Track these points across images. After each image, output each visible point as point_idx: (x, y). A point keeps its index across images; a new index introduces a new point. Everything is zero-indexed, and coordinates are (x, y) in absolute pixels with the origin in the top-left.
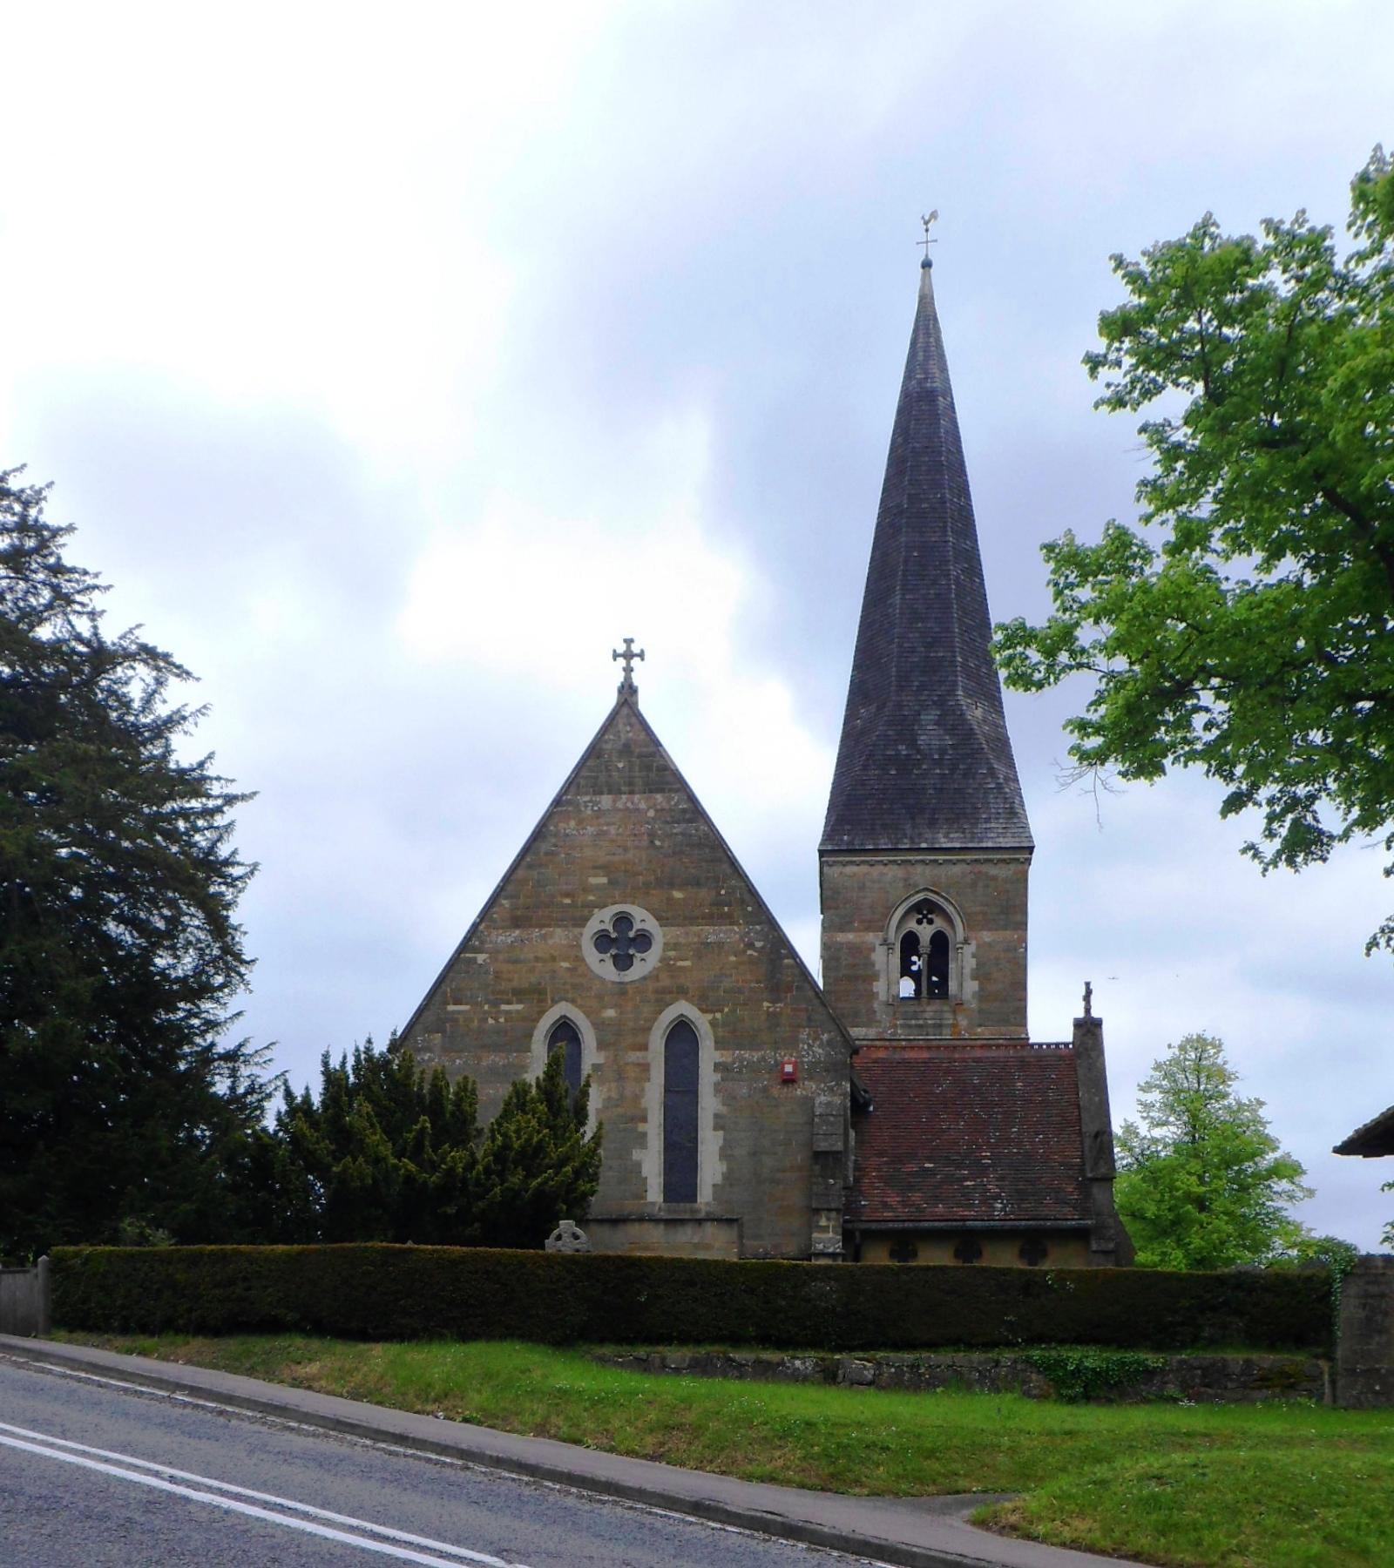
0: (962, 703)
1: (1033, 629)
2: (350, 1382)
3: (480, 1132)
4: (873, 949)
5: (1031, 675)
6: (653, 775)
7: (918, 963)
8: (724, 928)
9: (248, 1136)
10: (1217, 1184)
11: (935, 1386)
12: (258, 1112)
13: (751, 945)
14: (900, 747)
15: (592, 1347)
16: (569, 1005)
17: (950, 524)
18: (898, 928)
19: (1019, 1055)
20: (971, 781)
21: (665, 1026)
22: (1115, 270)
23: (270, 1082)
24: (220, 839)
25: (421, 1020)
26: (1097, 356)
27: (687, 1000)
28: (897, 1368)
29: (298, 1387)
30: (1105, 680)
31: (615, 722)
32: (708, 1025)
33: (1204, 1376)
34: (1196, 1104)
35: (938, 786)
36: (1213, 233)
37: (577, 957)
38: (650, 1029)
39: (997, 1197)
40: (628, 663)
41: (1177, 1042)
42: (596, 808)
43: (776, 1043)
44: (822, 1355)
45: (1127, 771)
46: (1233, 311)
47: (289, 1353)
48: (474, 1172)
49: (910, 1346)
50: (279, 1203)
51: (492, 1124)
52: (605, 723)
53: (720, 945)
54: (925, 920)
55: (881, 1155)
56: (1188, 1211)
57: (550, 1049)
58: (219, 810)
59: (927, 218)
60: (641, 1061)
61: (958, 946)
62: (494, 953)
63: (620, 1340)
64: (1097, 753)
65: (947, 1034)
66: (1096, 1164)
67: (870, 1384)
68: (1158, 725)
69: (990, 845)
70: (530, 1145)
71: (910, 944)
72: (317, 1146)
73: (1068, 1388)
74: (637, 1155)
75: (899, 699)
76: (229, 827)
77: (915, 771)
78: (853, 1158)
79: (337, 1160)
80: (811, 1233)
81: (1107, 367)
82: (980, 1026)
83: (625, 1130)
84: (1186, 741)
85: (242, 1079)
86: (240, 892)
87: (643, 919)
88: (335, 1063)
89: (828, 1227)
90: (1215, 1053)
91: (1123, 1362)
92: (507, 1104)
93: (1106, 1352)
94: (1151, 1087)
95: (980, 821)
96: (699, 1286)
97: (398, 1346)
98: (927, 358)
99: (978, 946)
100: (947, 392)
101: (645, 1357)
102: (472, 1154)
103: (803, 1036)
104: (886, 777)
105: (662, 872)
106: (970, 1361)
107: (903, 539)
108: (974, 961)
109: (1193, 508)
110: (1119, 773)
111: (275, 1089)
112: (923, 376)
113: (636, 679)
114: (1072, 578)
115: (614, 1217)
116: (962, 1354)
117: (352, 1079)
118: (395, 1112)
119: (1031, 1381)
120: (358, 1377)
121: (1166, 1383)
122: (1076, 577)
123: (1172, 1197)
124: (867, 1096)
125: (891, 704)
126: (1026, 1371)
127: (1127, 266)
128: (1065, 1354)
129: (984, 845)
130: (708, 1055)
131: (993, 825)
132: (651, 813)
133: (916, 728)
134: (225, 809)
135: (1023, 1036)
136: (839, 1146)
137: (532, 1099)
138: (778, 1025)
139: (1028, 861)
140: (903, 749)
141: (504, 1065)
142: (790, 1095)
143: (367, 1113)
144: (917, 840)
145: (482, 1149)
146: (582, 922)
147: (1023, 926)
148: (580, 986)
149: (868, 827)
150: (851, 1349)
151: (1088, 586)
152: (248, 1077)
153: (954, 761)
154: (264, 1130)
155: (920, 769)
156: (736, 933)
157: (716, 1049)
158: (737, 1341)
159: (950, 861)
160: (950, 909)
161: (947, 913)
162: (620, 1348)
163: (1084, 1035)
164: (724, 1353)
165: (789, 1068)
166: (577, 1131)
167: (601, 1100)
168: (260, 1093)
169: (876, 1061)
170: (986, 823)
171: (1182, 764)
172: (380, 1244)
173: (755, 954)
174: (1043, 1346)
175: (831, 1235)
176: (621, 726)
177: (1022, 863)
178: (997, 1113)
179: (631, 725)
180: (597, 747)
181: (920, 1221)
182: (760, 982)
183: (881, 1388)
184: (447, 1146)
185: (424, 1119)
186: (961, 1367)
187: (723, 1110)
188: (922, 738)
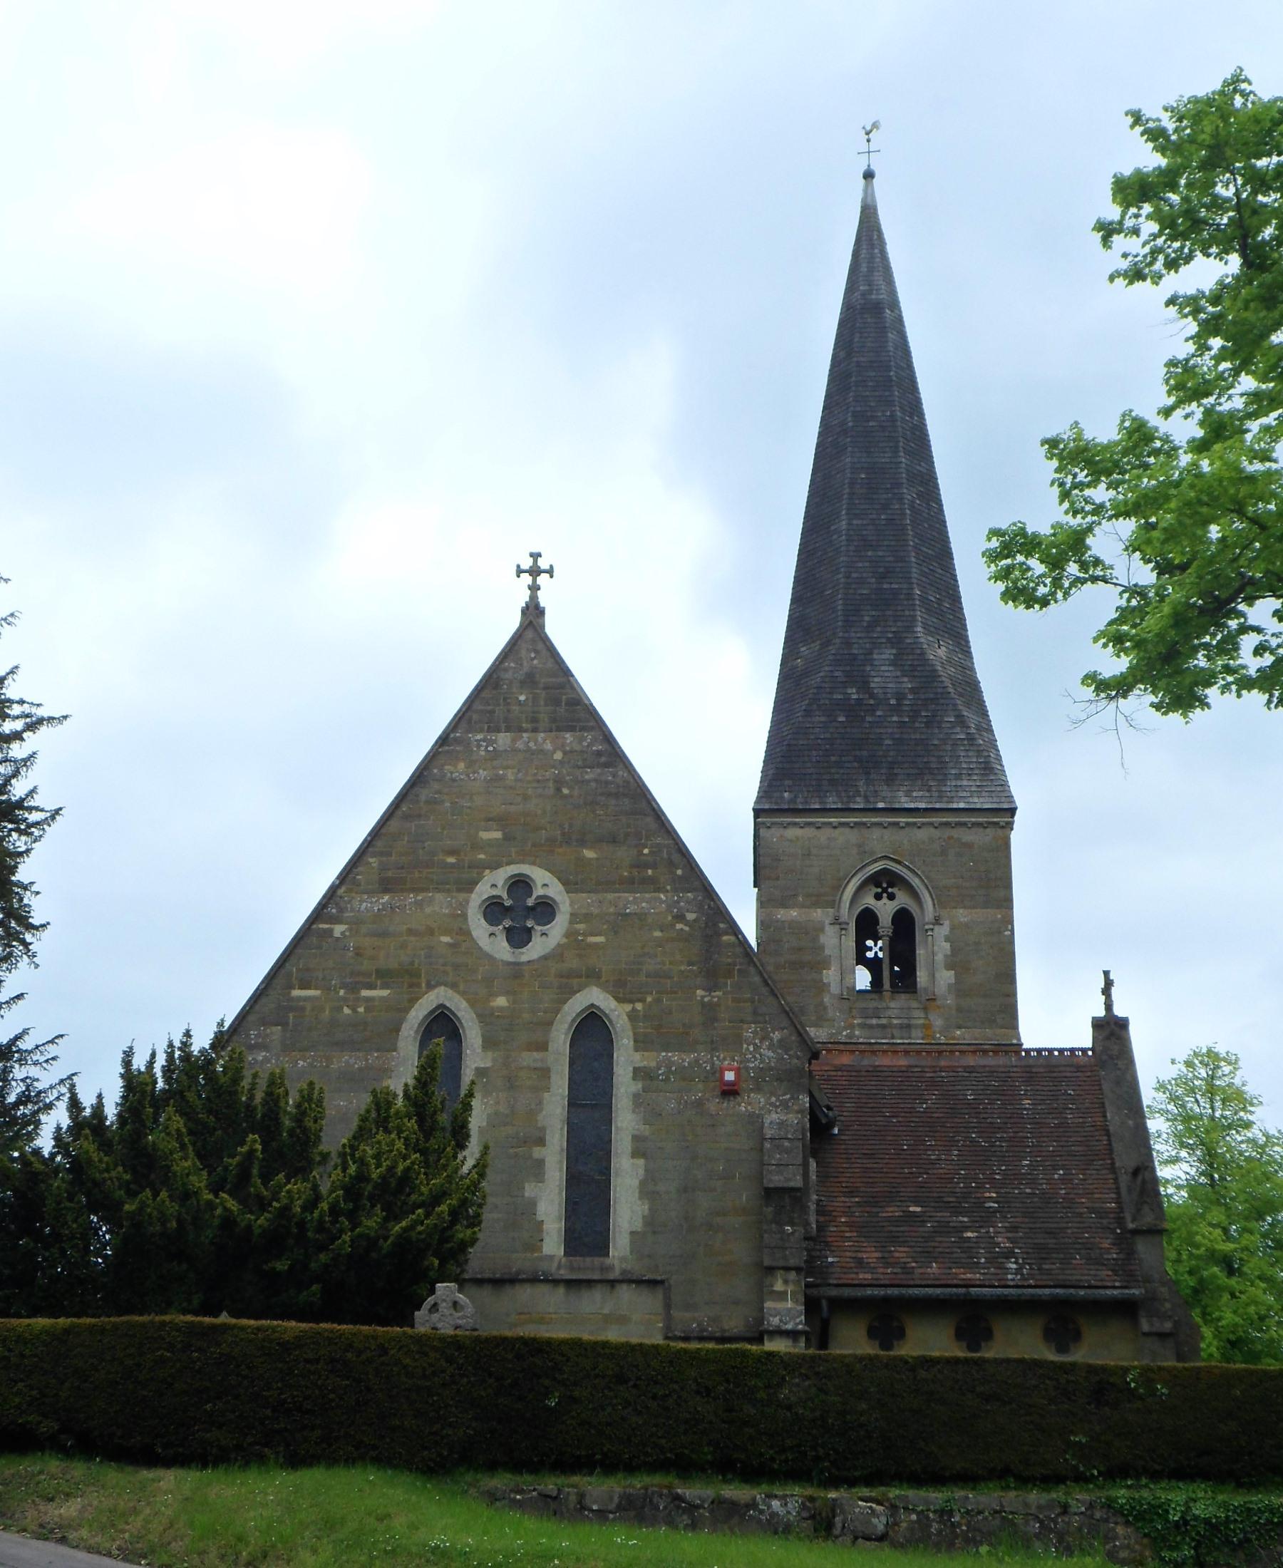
0: (922, 640)
1: (1035, 535)
2: (123, 1531)
3: (325, 1157)
4: (822, 930)
5: (1034, 590)
6: (562, 710)
7: (875, 949)
8: (647, 895)
9: (14, 1160)
10: (1247, 1240)
11: (977, 1544)
12: (30, 1128)
13: (680, 918)
14: (849, 691)
15: (479, 1476)
16: (450, 992)
17: (901, 444)
18: (853, 901)
20: (936, 731)
21: (570, 1019)
22: (1132, 127)
23: (52, 1087)
24: (16, 774)
25: (257, 1007)
26: (1111, 223)
27: (598, 986)
28: (918, 1514)
29: (46, 1539)
30: (1126, 595)
31: (516, 648)
32: (625, 1018)
35: (897, 736)
36: (1244, 90)
37: (461, 929)
38: (551, 1023)
39: (1009, 1254)
40: (534, 580)
41: (1182, 1056)
42: (491, 748)
43: (712, 1042)
44: (810, 1491)
45: (1161, 702)
46: (1268, 178)
47: (38, 1483)
48: (316, 1214)
49: (936, 1479)
50: (47, 1254)
51: (344, 1146)
53: (641, 916)
54: (885, 895)
55: (851, 1193)
56: (1214, 1276)
57: (423, 1045)
58: (17, 736)
59: (868, 128)
60: (539, 1065)
61: (927, 927)
62: (356, 924)
63: (518, 1466)
64: (1119, 683)
65: (917, 1038)
66: (1139, 1210)
67: (881, 1538)
68: (1195, 650)
69: (962, 805)
70: (393, 1175)
71: (867, 924)
72: (106, 1175)
73: (1171, 1548)
74: (530, 1190)
75: (846, 635)
76: (28, 760)
78: (815, 1197)
79: (132, 1194)
80: (762, 1302)
81: (1123, 235)
82: (959, 1027)
83: (516, 1155)
84: (1228, 670)
85: (14, 1083)
86: (35, 841)
87: (545, 883)
88: (139, 1063)
89: (785, 1293)
90: (1231, 1072)
91: (1249, 1510)
92: (364, 1119)
93: (1222, 1493)
96: (631, 1383)
97: (198, 1474)
98: (871, 270)
99: (953, 928)
100: (894, 305)
101: (555, 1494)
102: (315, 1188)
104: (834, 724)
105: (571, 826)
106: (1026, 1505)
108: (947, 946)
109: (1223, 400)
110: (1152, 705)
111: (58, 1099)
112: (867, 288)
114: (1082, 476)
115: (498, 1276)
116: (1012, 1494)
117: (160, 1084)
118: (215, 1129)
119: (1116, 1538)
120: (137, 1523)
122: (1086, 477)
123: (1191, 1255)
124: (831, 1114)
125: (838, 641)
126: (1106, 1521)
127: (1147, 121)
128: (1163, 1496)
129: (955, 806)
130: (626, 1059)
131: (965, 783)
132: (558, 756)
133: (868, 668)
134: (25, 735)
135: (1015, 1041)
136: (797, 1182)
137: (397, 1112)
138: (715, 1019)
139: (1010, 826)
140: (853, 693)
141: (360, 1069)
143: (178, 1130)
144: (872, 799)
145: (328, 1180)
146: (470, 886)
147: (1006, 903)
149: (814, 783)
150: (852, 1483)
151: (1103, 486)
152: (22, 1080)
153: (915, 708)
154: (37, 1152)
155: (873, 715)
156: (663, 902)
157: (636, 1050)
158: (685, 1467)
159: (915, 824)
160: (915, 882)
162: (518, 1479)
163: (1108, 1038)
164: (670, 1487)
165: (730, 1076)
166: (455, 1157)
167: (485, 1116)
168: (36, 1103)
170: (956, 779)
171: (1234, 694)
172: (182, 1317)
173: (687, 929)
175: (790, 1304)
176: (523, 653)
177: (1003, 827)
179: (536, 652)
180: (495, 676)
183: (896, 1545)
184: (281, 1176)
185: (254, 1141)
186: (1012, 1513)
187: (645, 1130)
188: (876, 680)
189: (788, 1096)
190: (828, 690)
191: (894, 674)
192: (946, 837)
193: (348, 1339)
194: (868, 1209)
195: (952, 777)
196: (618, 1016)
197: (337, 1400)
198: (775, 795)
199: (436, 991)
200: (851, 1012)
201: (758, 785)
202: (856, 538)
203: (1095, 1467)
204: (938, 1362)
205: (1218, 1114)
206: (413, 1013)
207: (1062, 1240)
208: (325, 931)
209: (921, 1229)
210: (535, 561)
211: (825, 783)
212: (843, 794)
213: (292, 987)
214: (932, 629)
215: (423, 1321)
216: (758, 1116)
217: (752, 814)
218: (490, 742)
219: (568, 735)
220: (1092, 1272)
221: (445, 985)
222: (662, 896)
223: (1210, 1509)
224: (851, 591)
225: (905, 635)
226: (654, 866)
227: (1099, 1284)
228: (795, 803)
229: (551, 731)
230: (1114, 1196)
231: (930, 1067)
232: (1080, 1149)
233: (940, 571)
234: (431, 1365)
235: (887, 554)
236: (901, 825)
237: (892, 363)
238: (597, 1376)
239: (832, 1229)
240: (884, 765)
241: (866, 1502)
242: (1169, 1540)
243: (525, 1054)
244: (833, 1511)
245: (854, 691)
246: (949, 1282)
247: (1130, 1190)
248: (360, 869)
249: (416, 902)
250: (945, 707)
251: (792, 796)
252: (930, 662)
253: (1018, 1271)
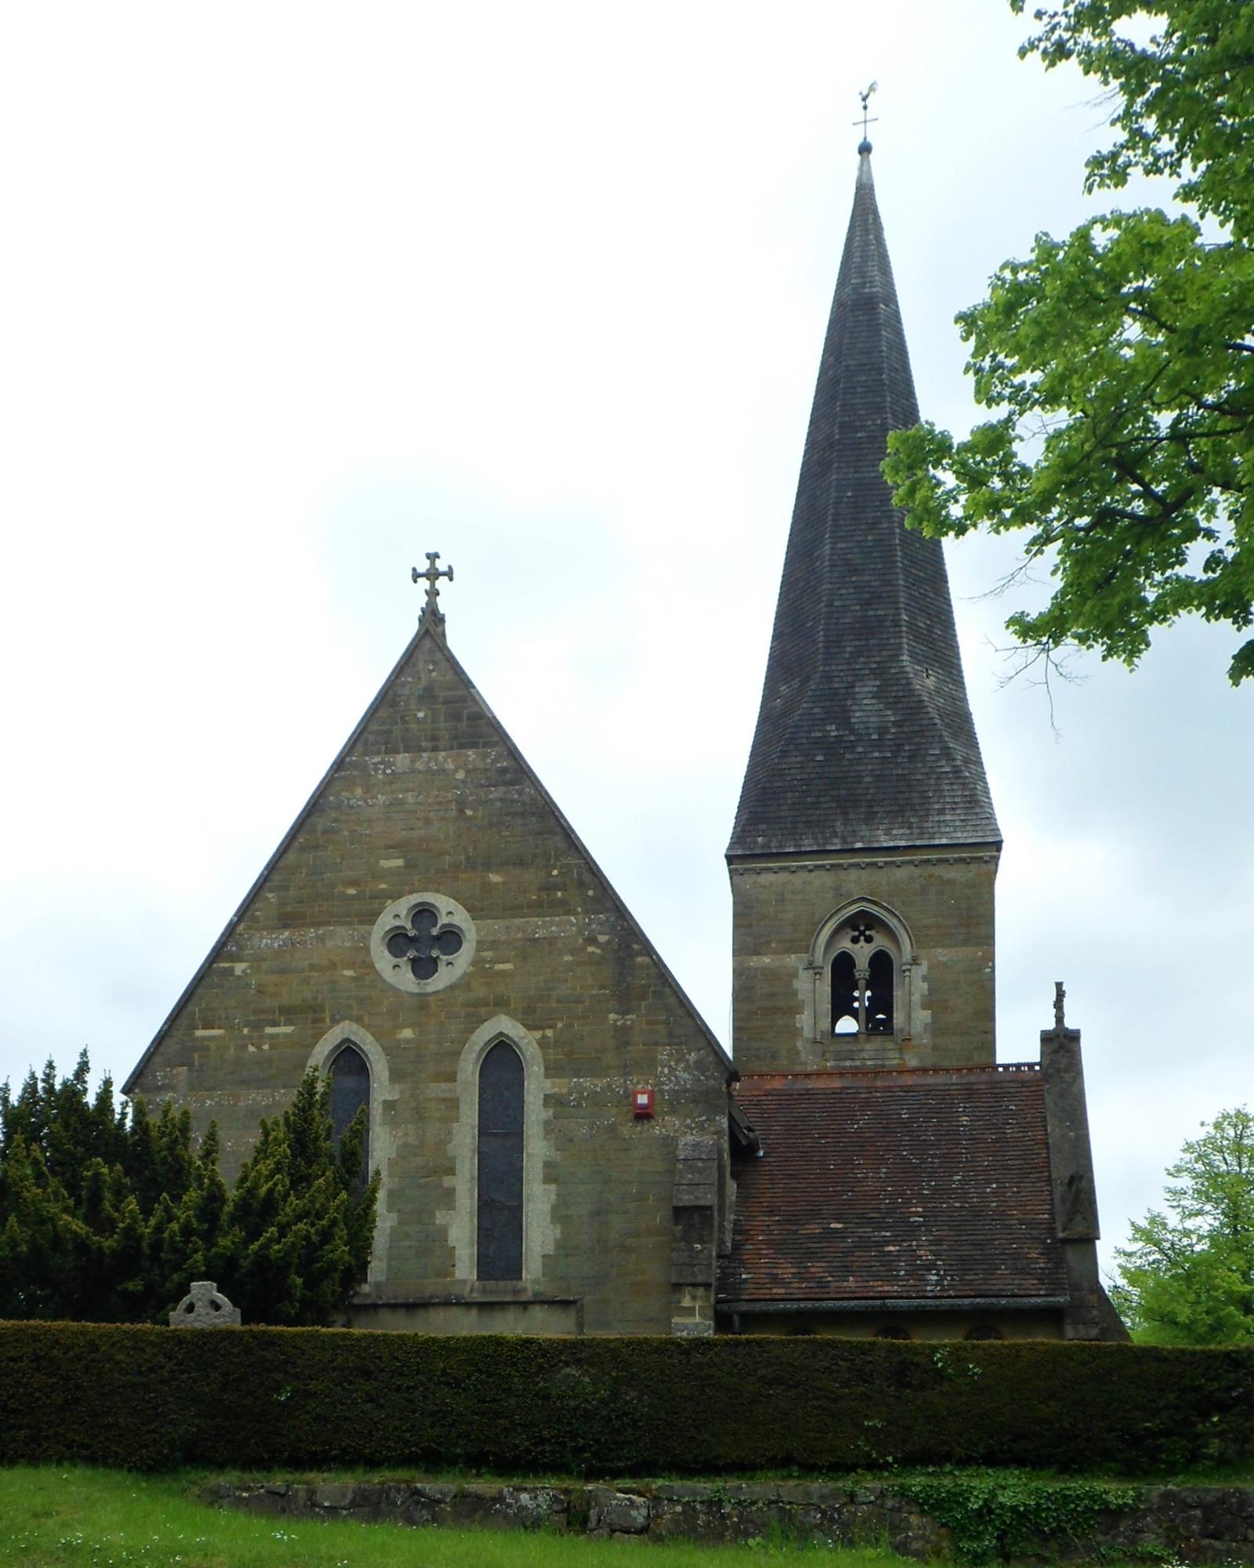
0: (908, 669)
11: (747, 1535)
13: (592, 940)
14: (828, 728)
19: (964, 1081)
21: (478, 1048)
25: (162, 1049)
31: (414, 659)
33: (1207, 1520)
34: (1236, 1189)
35: (878, 773)
37: (364, 962)
38: (459, 1053)
39: (930, 1267)
40: (433, 585)
43: (625, 1066)
44: (568, 1483)
49: (710, 1468)
52: (399, 662)
53: (551, 941)
54: (862, 938)
55: (771, 1213)
56: (1230, 1315)
59: (865, 93)
60: (448, 1095)
61: (904, 968)
62: (257, 961)
66: (1071, 1220)
67: (643, 1531)
69: (944, 841)
70: (253, 1196)
71: (843, 966)
73: (971, 1538)
74: (440, 1218)
77: (848, 756)
78: (733, 1217)
87: (450, 910)
89: (694, 1308)
91: (1066, 1497)
93: (1039, 1479)
94: (1178, 1171)
95: (932, 812)
98: (865, 258)
99: (930, 968)
100: (891, 298)
104: (811, 764)
106: (808, 1494)
107: (834, 477)
108: (925, 985)
112: (859, 281)
113: (443, 605)
115: (411, 1300)
116: (792, 1483)
119: (909, 1528)
121: (1139, 1531)
123: (1210, 1297)
124: (751, 1135)
125: (818, 675)
126: (899, 1510)
128: (964, 1481)
129: (937, 842)
130: (536, 1086)
131: (948, 818)
132: (460, 775)
136: (710, 1199)
138: (627, 1043)
139: (995, 860)
140: (833, 730)
142: (645, 1135)
144: (850, 840)
146: (371, 918)
150: (616, 1474)
153: (898, 742)
155: (853, 752)
156: (573, 925)
157: (547, 1076)
158: (433, 1461)
159: (893, 863)
160: (893, 922)
161: (891, 929)
162: (247, 1476)
163: (1056, 1052)
165: (643, 1099)
169: (769, 1093)
173: (598, 951)
174: (931, 1469)
175: (698, 1319)
178: (933, 1156)
179: (434, 663)
180: (391, 693)
182: (604, 987)
183: (659, 1539)
186: (790, 1503)
187: (557, 1157)
188: (857, 714)
189: (704, 1118)
190: (806, 728)
191: (876, 708)
192: (926, 874)
193: (54, 1335)
194: (787, 1227)
195: (935, 812)
196: (528, 1044)
197: (44, 1398)
198: (749, 840)
199: (341, 1025)
200: (824, 1055)
201: (731, 831)
202: (839, 563)
203: (890, 1454)
204: (716, 1345)
205: (1244, 1170)
206: (318, 1048)
207: (989, 1252)
208: (225, 969)
209: (842, 1245)
210: (433, 563)
211: (801, 825)
212: (819, 836)
214: (920, 657)
215: (179, 1319)
216: (673, 1138)
217: (725, 861)
218: (388, 765)
219: (470, 753)
220: (1016, 1282)
221: (350, 1019)
222: (573, 919)
223: (1020, 1496)
224: (833, 621)
225: (889, 665)
227: (1022, 1293)
228: (769, 847)
229: (452, 749)
230: (1048, 1207)
231: (867, 1088)
232: (1019, 1162)
233: (932, 595)
234: (147, 1361)
235: (872, 578)
236: (880, 864)
237: (885, 365)
238: (334, 1369)
239: (748, 1247)
240: (863, 804)
241: (627, 1493)
242: (969, 1530)
243: (433, 1085)
244: (588, 1503)
245: (834, 728)
246: (865, 1295)
247: (1063, 1200)
248: (258, 905)
249: (317, 937)
250: (930, 740)
251: (766, 839)
252: (916, 693)
253: (938, 1283)
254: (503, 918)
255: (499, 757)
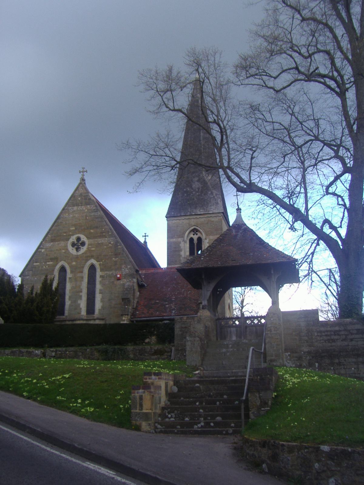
8: (103, 239)
13: (110, 243)
18: (188, 236)
27: (93, 259)
32: (99, 265)
38: (84, 267)
39: (174, 309)
40: (83, 174)
53: (102, 243)
60: (82, 276)
62: (46, 249)
69: (211, 212)
71: (191, 240)
74: (79, 302)
78: (137, 300)
87: (83, 238)
99: (209, 240)
103: (123, 267)
130: (99, 273)
132: (86, 210)
138: (116, 264)
144: (191, 212)
146: (68, 240)
148: (67, 257)
160: (201, 230)
165: (118, 276)
173: (111, 245)
179: (82, 189)
181: (142, 318)
182: (112, 253)
187: (102, 288)
213: (33, 263)
226: (105, 233)
243: (79, 274)
253: (174, 313)
254: (93, 239)
255: (94, 207)
